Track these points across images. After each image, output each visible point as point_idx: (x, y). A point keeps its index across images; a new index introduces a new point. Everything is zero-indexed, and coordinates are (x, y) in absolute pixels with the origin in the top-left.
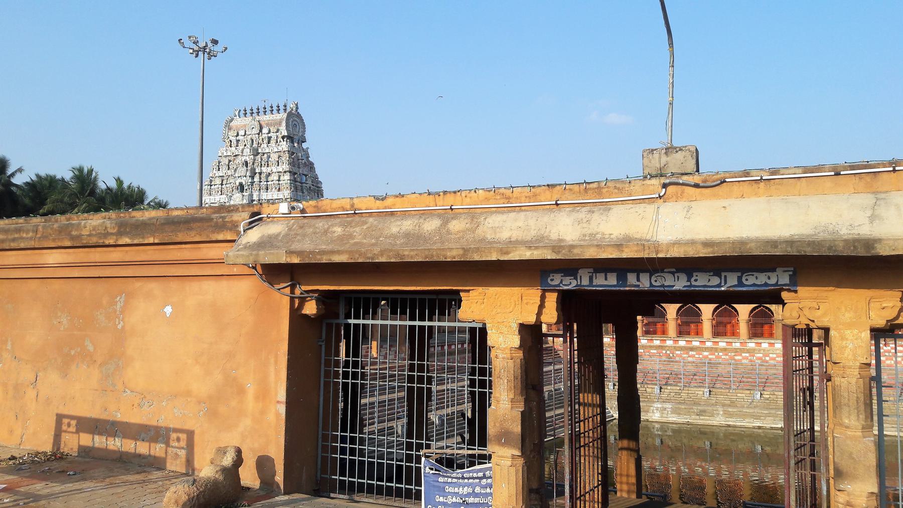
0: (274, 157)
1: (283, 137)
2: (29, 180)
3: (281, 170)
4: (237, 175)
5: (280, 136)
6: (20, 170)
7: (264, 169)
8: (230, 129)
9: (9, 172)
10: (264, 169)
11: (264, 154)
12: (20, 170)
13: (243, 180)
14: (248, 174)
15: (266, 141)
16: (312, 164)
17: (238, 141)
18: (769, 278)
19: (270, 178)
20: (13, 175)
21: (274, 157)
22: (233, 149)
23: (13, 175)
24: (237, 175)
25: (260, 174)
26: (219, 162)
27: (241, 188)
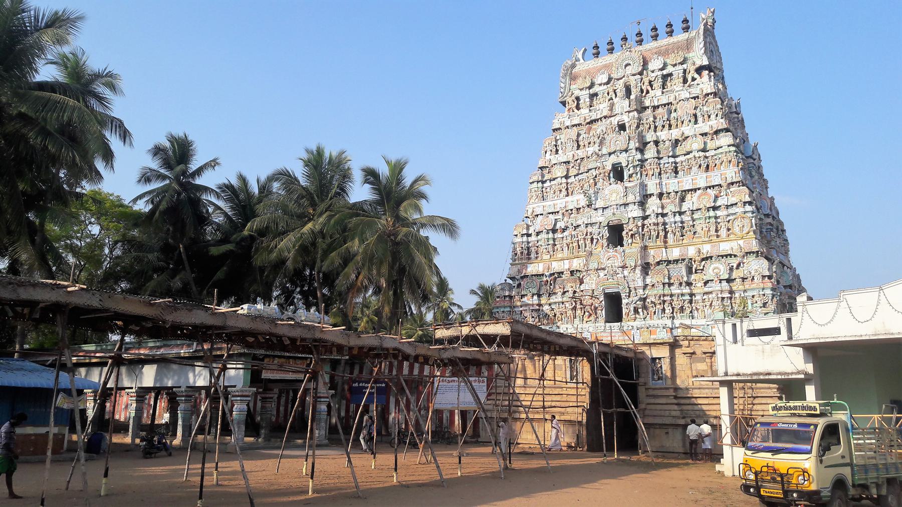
0: (684, 110)
1: (699, 70)
2: (226, 182)
3: (706, 129)
4: (605, 151)
5: (692, 69)
6: (213, 164)
7: (663, 135)
8: (574, 78)
9: (193, 166)
10: (663, 135)
11: (655, 108)
12: (213, 164)
13: (622, 159)
14: (633, 145)
15: (657, 84)
16: (742, 121)
17: (593, 96)
18: (614, 214)
19: (679, 150)
20: (199, 172)
22: (584, 111)
23: (199, 172)
24: (605, 151)
25: (656, 143)
26: (556, 141)
27: (618, 173)
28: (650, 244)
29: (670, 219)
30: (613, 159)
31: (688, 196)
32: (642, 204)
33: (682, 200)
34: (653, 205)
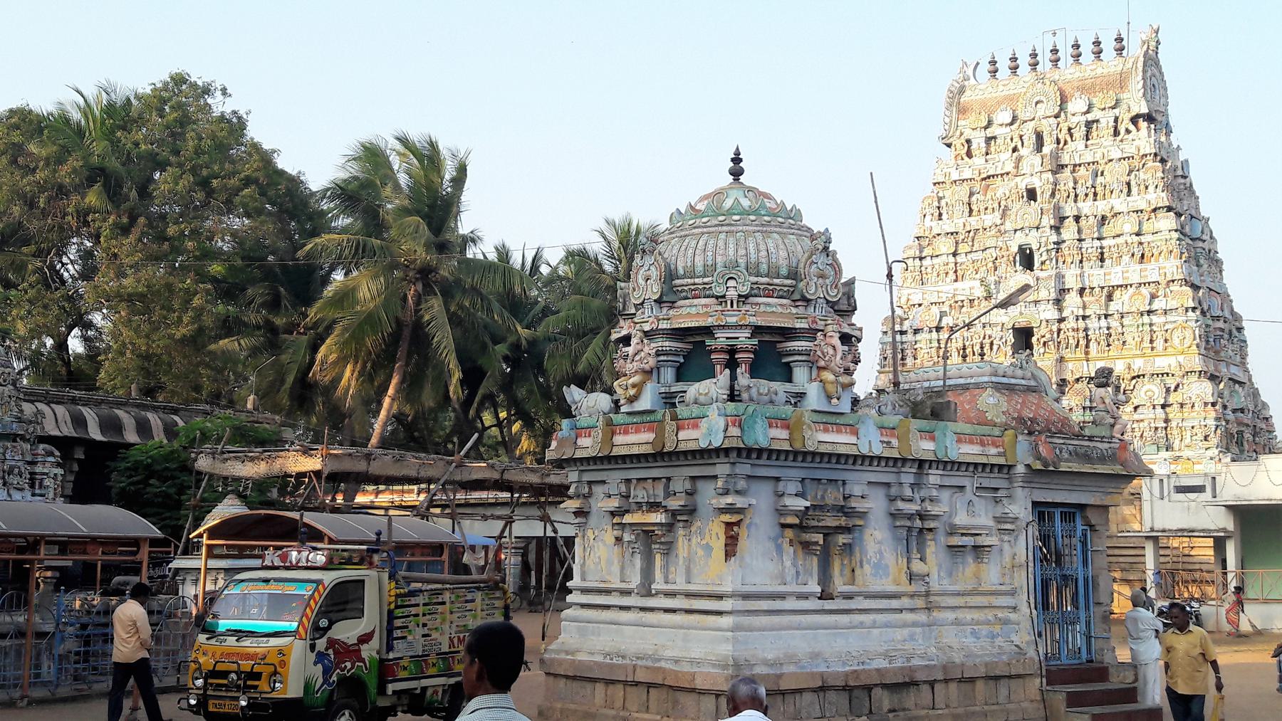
13: (1032, 240)
21: (1114, 175)
28: (1067, 354)
29: (1093, 324)
30: (1020, 239)
31: (1117, 294)
32: (1058, 302)
33: (1110, 298)
34: (1072, 300)
